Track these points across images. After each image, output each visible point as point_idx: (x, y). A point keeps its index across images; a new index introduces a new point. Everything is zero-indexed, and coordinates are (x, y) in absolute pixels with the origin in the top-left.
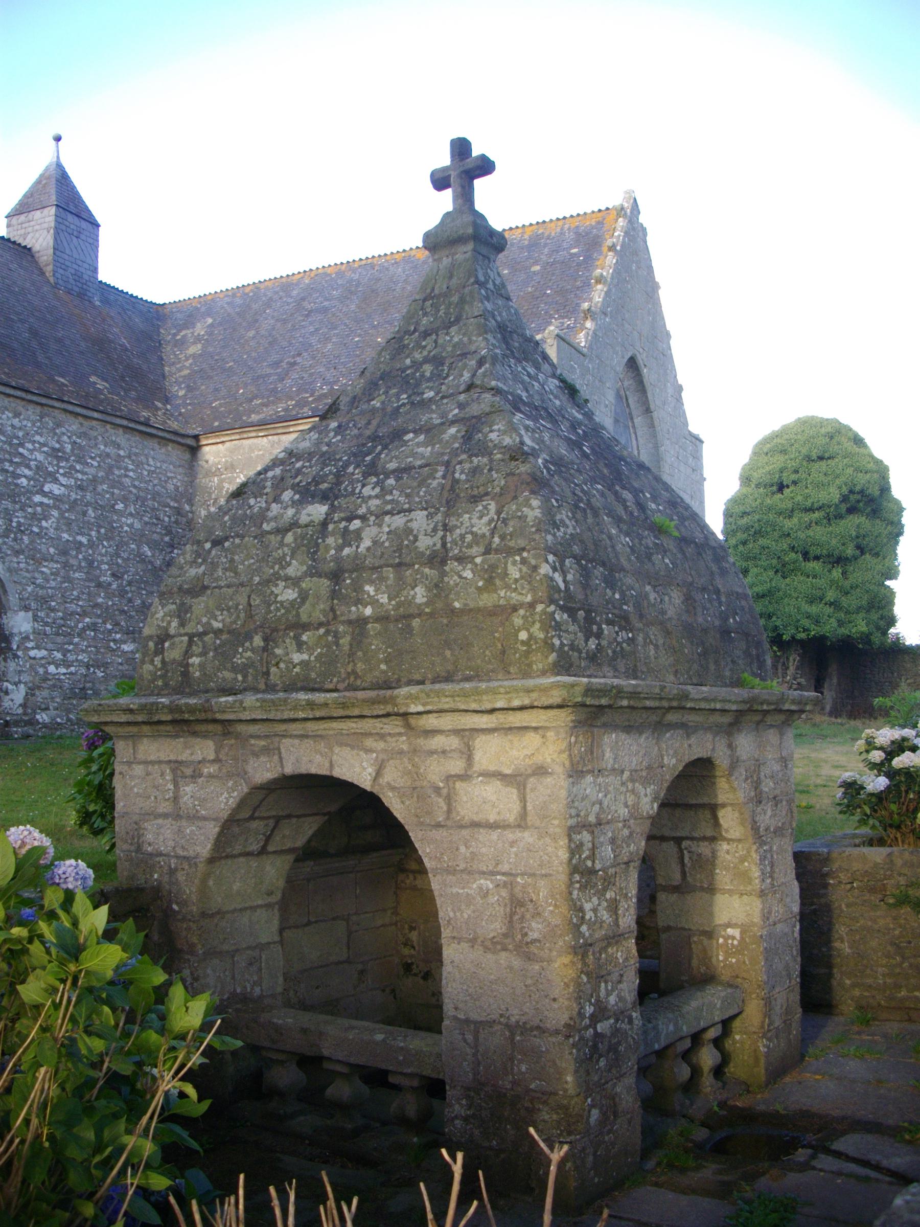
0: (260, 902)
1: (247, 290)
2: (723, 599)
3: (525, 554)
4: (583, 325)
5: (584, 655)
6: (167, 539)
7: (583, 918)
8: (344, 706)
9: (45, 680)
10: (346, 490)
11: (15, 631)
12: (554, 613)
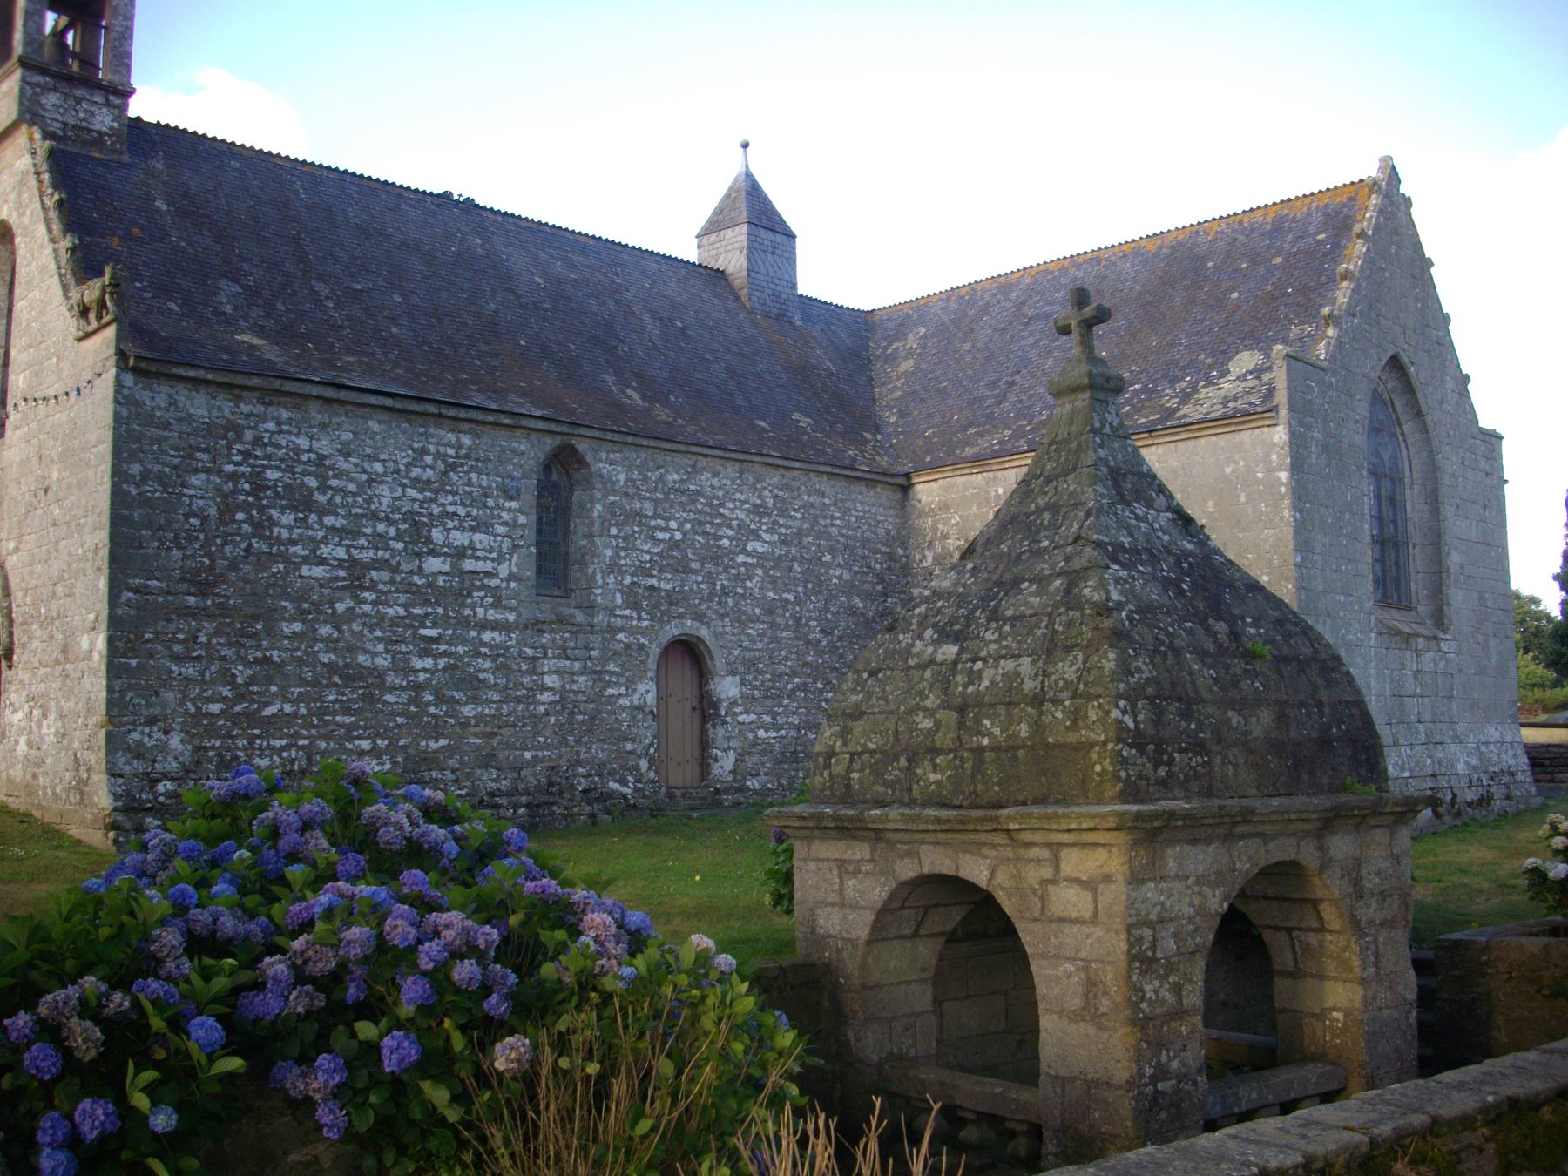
1: (963, 292)
2: (1327, 710)
6: (879, 588)
8: (962, 822)
9: (755, 744)
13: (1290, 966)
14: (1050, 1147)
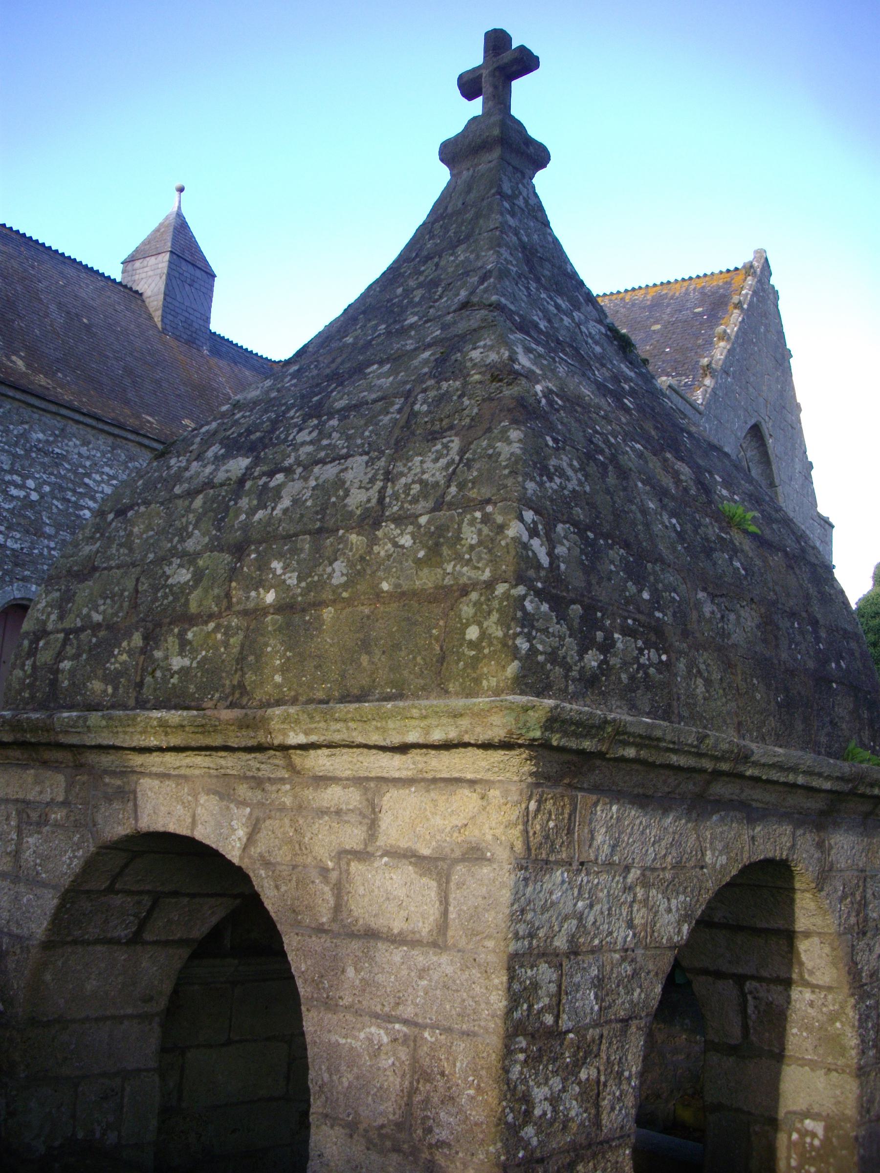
0: (129, 1011)
2: (823, 635)
3: (489, 509)
4: (702, 382)
5: (574, 674)
7: (528, 1113)
10: (278, 438)
12: (524, 597)
13: (735, 1033)
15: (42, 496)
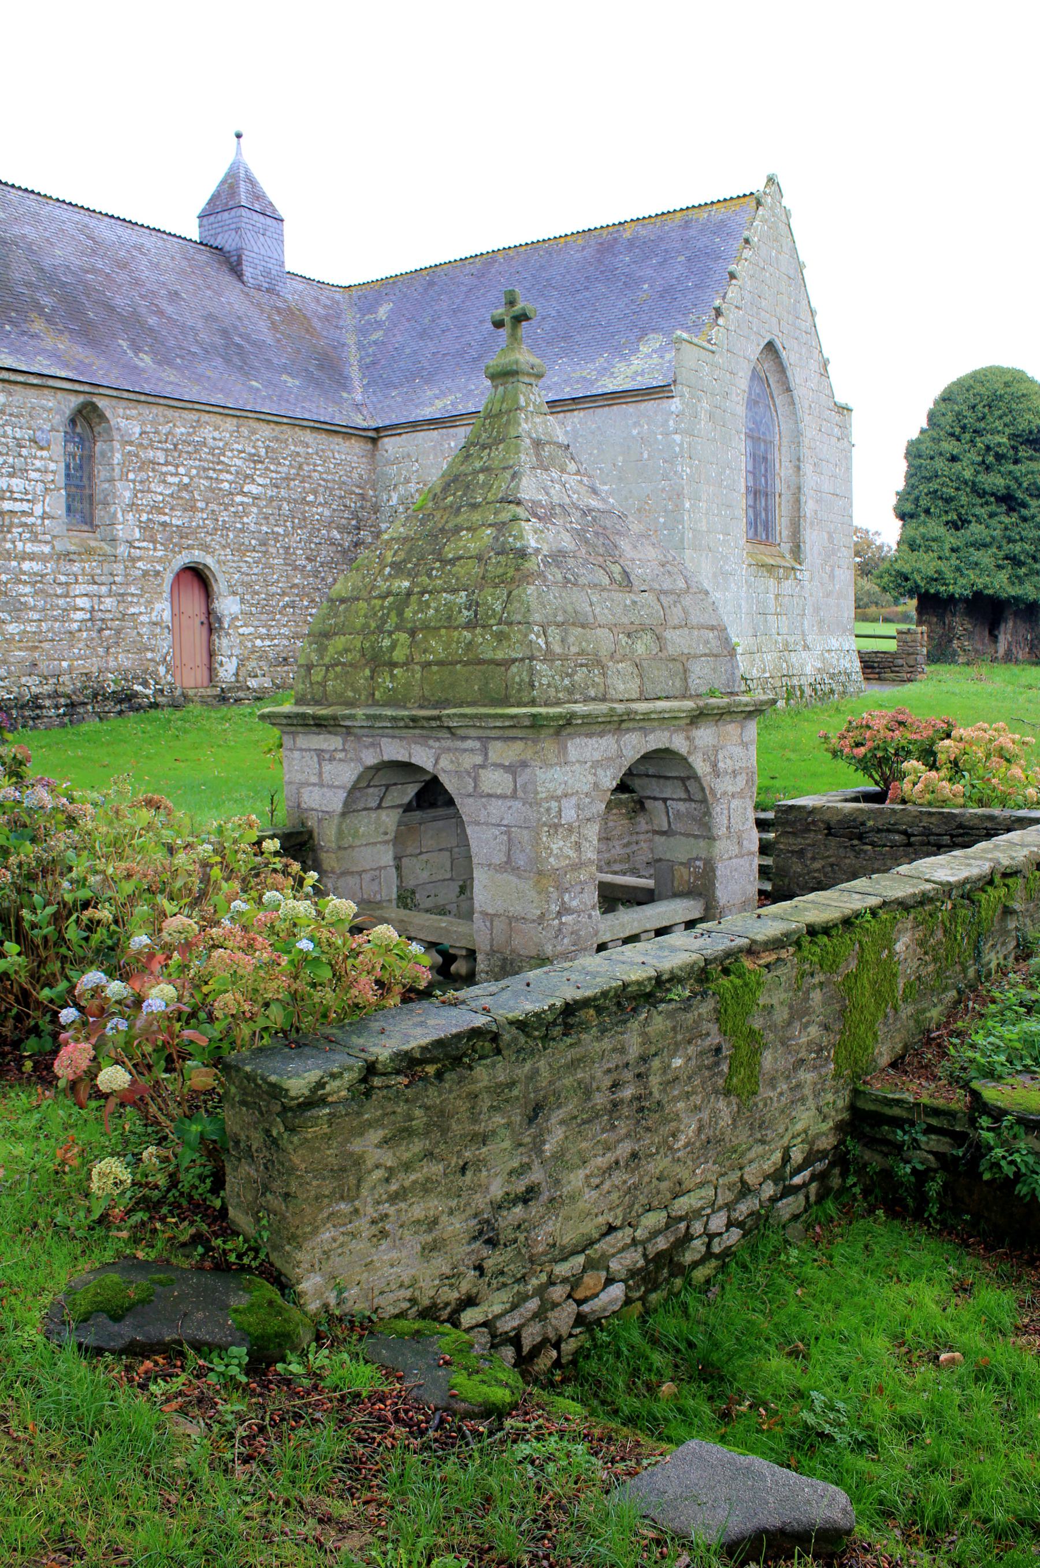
6: (354, 522)
11: (226, 613)
14: (481, 965)
15: (191, 478)
